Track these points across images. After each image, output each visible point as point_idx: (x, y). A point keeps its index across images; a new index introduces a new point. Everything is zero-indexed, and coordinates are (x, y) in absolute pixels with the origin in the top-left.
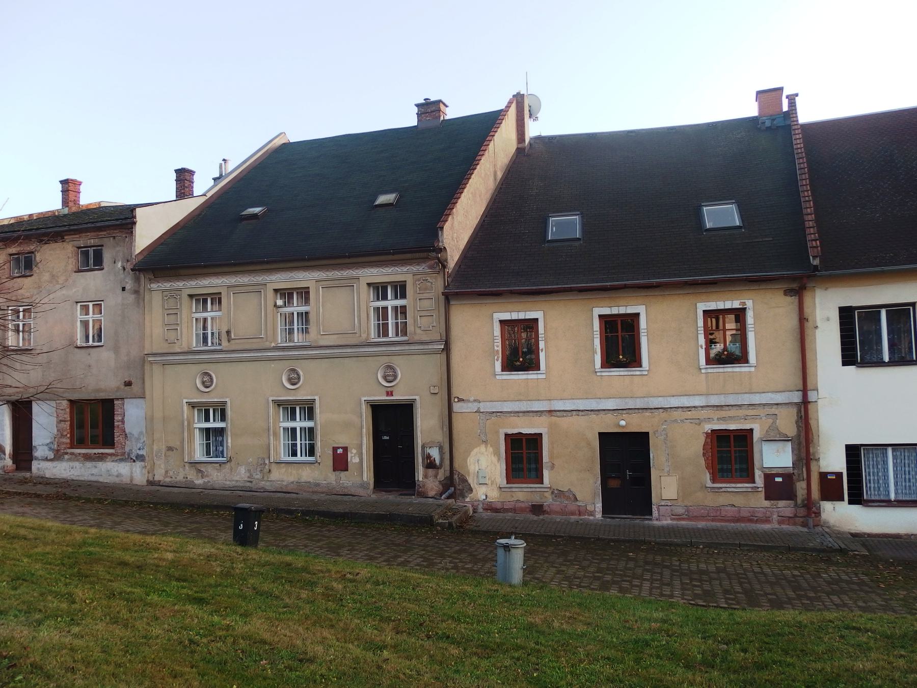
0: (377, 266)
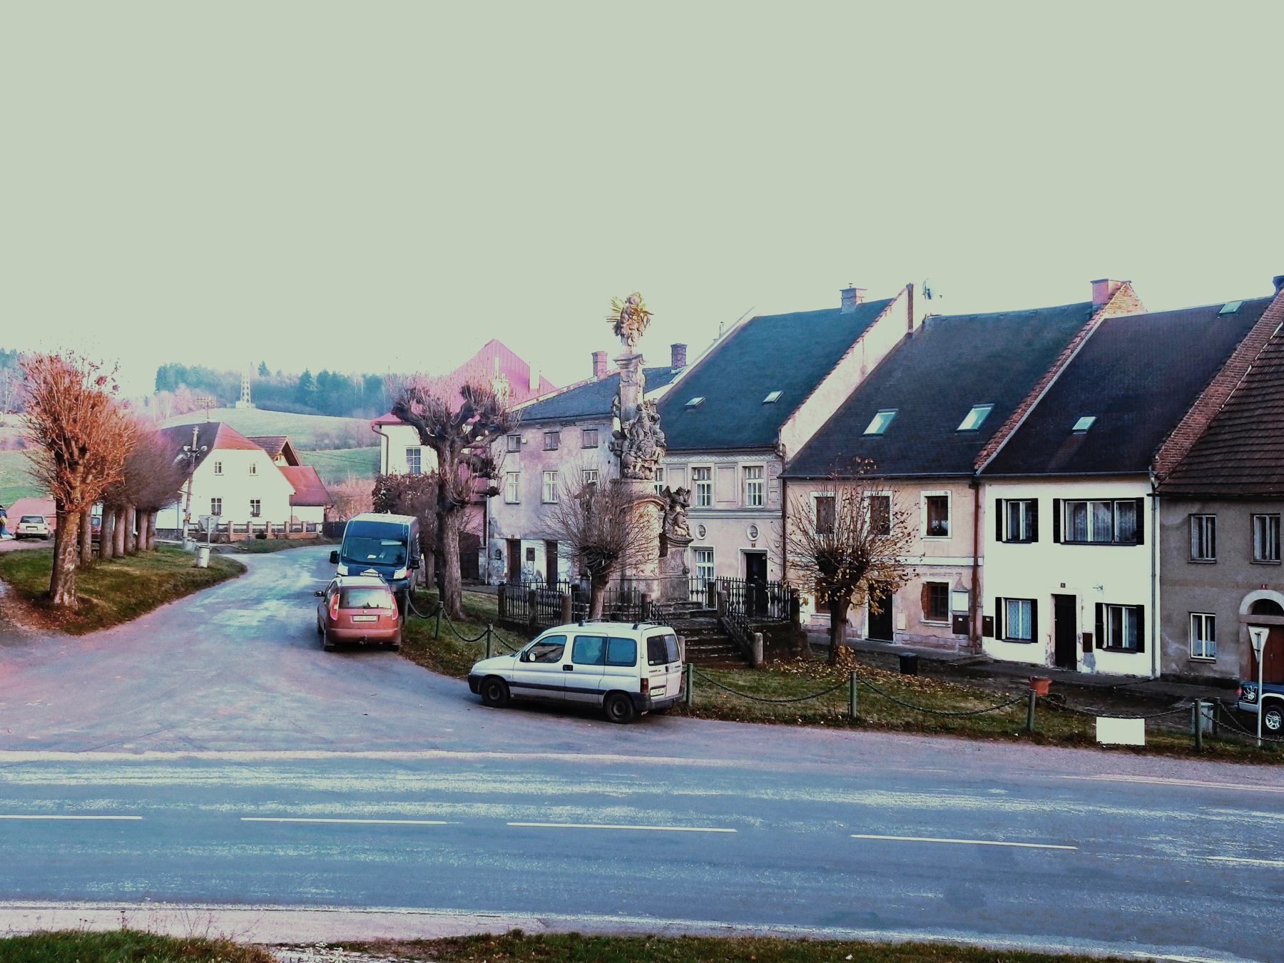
0: (744, 455)
